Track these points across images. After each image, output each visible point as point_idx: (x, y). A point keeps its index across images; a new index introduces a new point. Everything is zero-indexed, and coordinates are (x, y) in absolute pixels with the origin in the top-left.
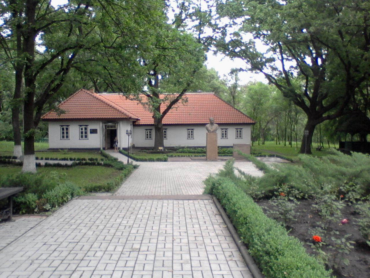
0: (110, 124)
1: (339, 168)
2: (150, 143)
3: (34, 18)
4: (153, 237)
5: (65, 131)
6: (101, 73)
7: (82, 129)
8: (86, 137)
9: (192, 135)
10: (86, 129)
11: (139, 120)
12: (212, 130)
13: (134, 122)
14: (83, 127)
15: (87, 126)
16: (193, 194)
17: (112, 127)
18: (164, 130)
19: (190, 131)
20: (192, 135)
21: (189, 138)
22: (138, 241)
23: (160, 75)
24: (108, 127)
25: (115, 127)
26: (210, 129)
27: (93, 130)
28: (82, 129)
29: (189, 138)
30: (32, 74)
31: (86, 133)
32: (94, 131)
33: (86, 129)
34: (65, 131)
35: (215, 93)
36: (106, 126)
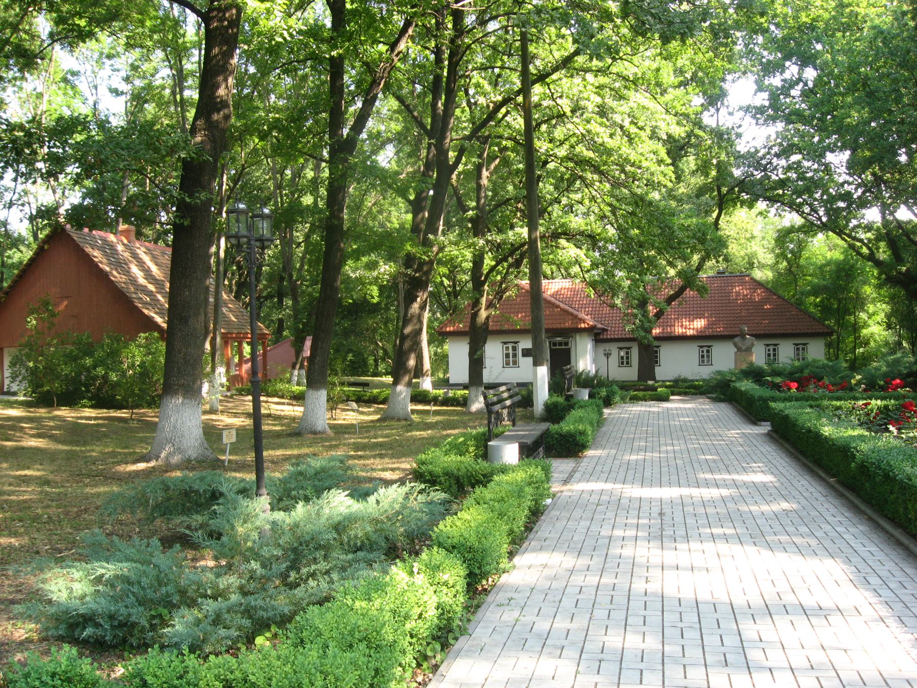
2: (631, 373)
3: (450, 178)
4: (650, 599)
7: (507, 348)
8: (515, 363)
9: (708, 356)
10: (514, 349)
11: (607, 330)
12: (744, 348)
13: (599, 334)
15: (516, 343)
16: (781, 559)
17: (560, 344)
19: (705, 349)
20: (708, 356)
21: (702, 363)
24: (555, 344)
25: (566, 344)
26: (740, 344)
28: (507, 348)
29: (702, 363)
30: (184, 118)
31: (515, 355)
33: (514, 349)
35: (433, 525)
36: (550, 342)
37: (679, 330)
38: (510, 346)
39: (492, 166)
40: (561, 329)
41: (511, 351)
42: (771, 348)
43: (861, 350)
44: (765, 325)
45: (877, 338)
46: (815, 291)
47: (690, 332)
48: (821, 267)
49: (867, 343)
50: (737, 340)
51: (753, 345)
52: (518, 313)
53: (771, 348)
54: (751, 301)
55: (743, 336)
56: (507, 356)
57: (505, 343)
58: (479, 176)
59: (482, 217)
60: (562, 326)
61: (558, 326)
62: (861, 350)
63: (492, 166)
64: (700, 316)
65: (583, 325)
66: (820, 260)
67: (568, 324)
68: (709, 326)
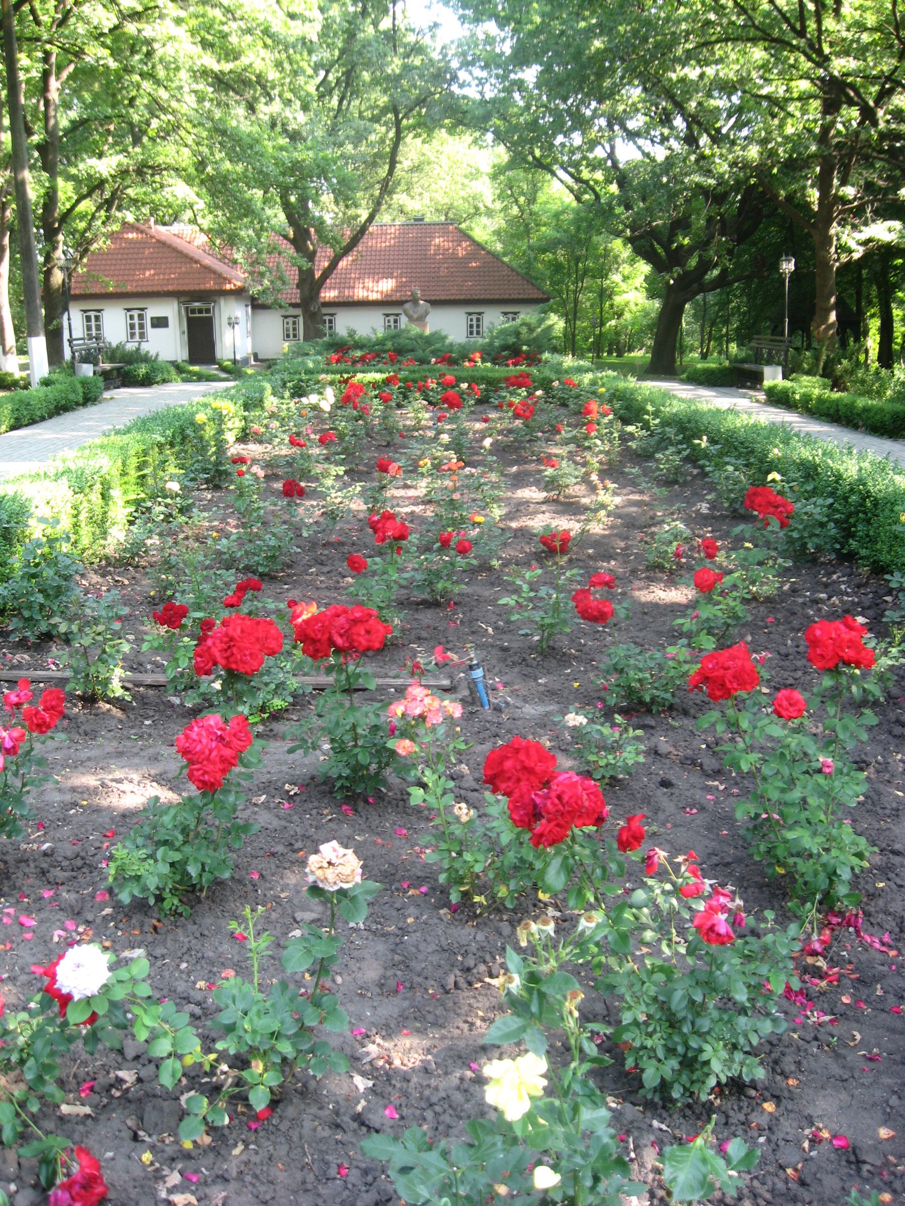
0: (197, 304)
1: (411, 493)
5: (93, 323)
6: (539, 747)
7: (132, 317)
8: (142, 335)
10: (141, 317)
14: (136, 313)
17: (200, 311)
18: (327, 318)
19: (392, 318)
22: (639, 148)
23: (532, 1187)
24: (193, 311)
25: (208, 311)
27: (158, 318)
28: (132, 317)
31: (142, 326)
32: (160, 323)
33: (141, 317)
34: (93, 323)
37: (360, 293)
38: (136, 313)
39: (65, 75)
40: (200, 291)
41: (136, 321)
42: (474, 317)
43: (613, 323)
44: (470, 288)
45: (634, 309)
46: (550, 246)
47: (374, 296)
48: (557, 215)
49: (620, 315)
50: (407, 306)
51: (427, 313)
52: (145, 269)
53: (474, 317)
54: (454, 256)
55: (415, 301)
56: (132, 327)
57: (129, 310)
58: (45, 89)
59: (52, 144)
60: (202, 287)
61: (197, 288)
62: (613, 323)
63: (65, 75)
64: (388, 275)
65: (228, 287)
66: (554, 207)
67: (211, 285)
68: (399, 287)
